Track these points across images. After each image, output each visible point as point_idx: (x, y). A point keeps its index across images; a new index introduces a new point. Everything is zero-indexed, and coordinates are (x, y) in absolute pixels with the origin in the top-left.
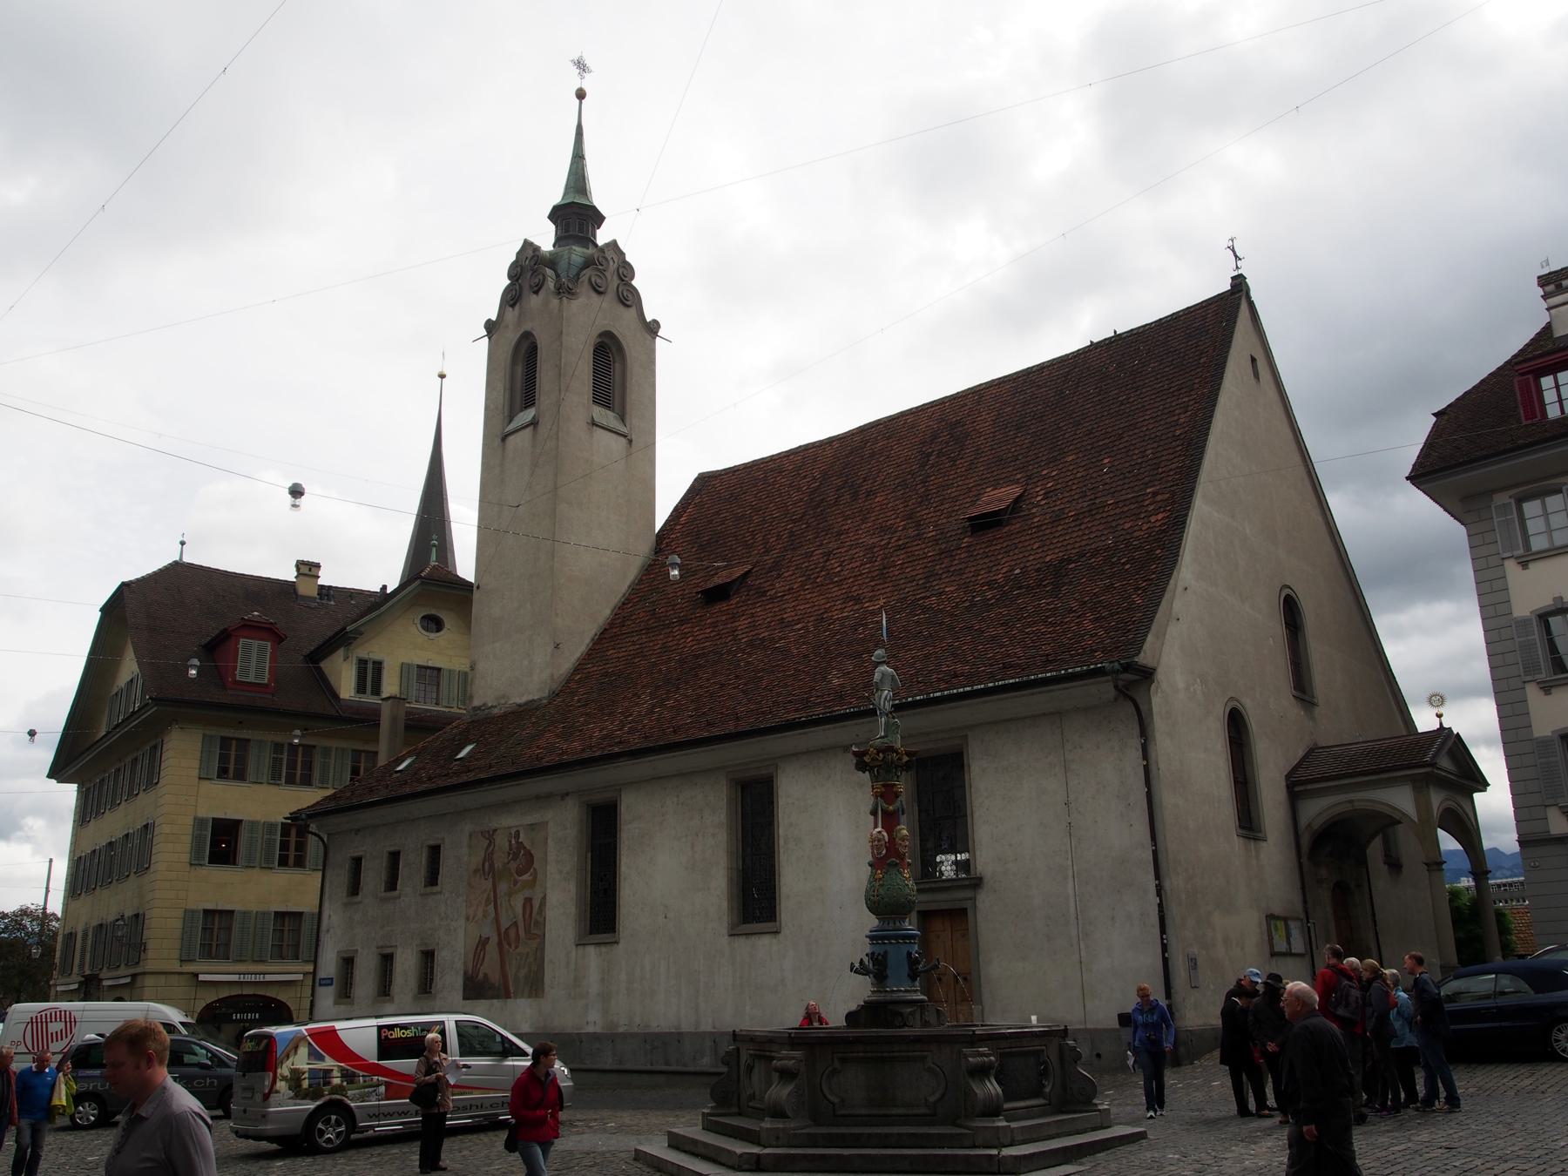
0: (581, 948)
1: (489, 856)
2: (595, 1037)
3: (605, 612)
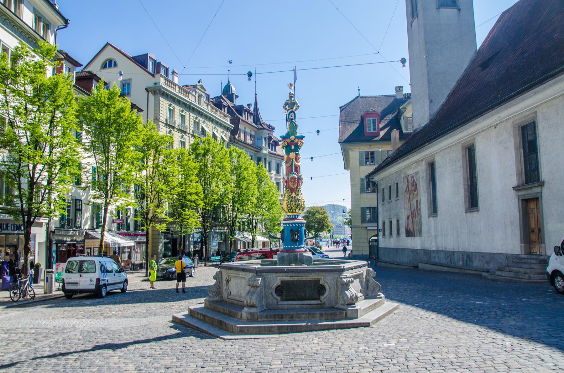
1: (408, 186)
2: (434, 251)
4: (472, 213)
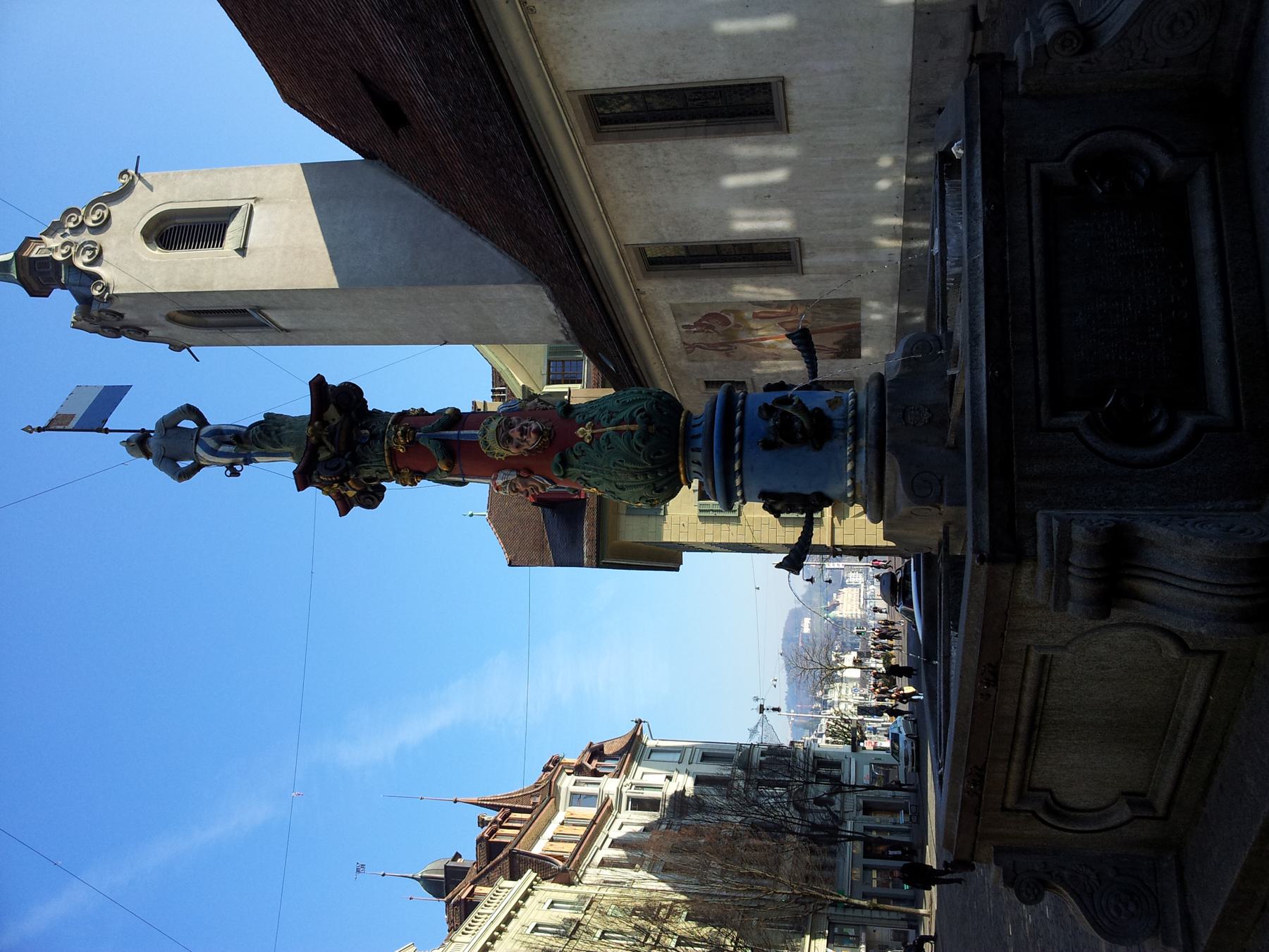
0: (805, 271)
1: (714, 347)
3: (447, 221)
4: (791, 107)
